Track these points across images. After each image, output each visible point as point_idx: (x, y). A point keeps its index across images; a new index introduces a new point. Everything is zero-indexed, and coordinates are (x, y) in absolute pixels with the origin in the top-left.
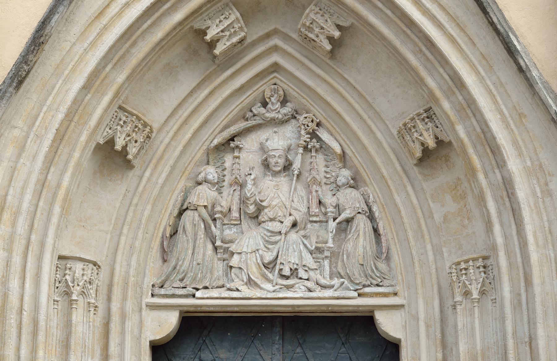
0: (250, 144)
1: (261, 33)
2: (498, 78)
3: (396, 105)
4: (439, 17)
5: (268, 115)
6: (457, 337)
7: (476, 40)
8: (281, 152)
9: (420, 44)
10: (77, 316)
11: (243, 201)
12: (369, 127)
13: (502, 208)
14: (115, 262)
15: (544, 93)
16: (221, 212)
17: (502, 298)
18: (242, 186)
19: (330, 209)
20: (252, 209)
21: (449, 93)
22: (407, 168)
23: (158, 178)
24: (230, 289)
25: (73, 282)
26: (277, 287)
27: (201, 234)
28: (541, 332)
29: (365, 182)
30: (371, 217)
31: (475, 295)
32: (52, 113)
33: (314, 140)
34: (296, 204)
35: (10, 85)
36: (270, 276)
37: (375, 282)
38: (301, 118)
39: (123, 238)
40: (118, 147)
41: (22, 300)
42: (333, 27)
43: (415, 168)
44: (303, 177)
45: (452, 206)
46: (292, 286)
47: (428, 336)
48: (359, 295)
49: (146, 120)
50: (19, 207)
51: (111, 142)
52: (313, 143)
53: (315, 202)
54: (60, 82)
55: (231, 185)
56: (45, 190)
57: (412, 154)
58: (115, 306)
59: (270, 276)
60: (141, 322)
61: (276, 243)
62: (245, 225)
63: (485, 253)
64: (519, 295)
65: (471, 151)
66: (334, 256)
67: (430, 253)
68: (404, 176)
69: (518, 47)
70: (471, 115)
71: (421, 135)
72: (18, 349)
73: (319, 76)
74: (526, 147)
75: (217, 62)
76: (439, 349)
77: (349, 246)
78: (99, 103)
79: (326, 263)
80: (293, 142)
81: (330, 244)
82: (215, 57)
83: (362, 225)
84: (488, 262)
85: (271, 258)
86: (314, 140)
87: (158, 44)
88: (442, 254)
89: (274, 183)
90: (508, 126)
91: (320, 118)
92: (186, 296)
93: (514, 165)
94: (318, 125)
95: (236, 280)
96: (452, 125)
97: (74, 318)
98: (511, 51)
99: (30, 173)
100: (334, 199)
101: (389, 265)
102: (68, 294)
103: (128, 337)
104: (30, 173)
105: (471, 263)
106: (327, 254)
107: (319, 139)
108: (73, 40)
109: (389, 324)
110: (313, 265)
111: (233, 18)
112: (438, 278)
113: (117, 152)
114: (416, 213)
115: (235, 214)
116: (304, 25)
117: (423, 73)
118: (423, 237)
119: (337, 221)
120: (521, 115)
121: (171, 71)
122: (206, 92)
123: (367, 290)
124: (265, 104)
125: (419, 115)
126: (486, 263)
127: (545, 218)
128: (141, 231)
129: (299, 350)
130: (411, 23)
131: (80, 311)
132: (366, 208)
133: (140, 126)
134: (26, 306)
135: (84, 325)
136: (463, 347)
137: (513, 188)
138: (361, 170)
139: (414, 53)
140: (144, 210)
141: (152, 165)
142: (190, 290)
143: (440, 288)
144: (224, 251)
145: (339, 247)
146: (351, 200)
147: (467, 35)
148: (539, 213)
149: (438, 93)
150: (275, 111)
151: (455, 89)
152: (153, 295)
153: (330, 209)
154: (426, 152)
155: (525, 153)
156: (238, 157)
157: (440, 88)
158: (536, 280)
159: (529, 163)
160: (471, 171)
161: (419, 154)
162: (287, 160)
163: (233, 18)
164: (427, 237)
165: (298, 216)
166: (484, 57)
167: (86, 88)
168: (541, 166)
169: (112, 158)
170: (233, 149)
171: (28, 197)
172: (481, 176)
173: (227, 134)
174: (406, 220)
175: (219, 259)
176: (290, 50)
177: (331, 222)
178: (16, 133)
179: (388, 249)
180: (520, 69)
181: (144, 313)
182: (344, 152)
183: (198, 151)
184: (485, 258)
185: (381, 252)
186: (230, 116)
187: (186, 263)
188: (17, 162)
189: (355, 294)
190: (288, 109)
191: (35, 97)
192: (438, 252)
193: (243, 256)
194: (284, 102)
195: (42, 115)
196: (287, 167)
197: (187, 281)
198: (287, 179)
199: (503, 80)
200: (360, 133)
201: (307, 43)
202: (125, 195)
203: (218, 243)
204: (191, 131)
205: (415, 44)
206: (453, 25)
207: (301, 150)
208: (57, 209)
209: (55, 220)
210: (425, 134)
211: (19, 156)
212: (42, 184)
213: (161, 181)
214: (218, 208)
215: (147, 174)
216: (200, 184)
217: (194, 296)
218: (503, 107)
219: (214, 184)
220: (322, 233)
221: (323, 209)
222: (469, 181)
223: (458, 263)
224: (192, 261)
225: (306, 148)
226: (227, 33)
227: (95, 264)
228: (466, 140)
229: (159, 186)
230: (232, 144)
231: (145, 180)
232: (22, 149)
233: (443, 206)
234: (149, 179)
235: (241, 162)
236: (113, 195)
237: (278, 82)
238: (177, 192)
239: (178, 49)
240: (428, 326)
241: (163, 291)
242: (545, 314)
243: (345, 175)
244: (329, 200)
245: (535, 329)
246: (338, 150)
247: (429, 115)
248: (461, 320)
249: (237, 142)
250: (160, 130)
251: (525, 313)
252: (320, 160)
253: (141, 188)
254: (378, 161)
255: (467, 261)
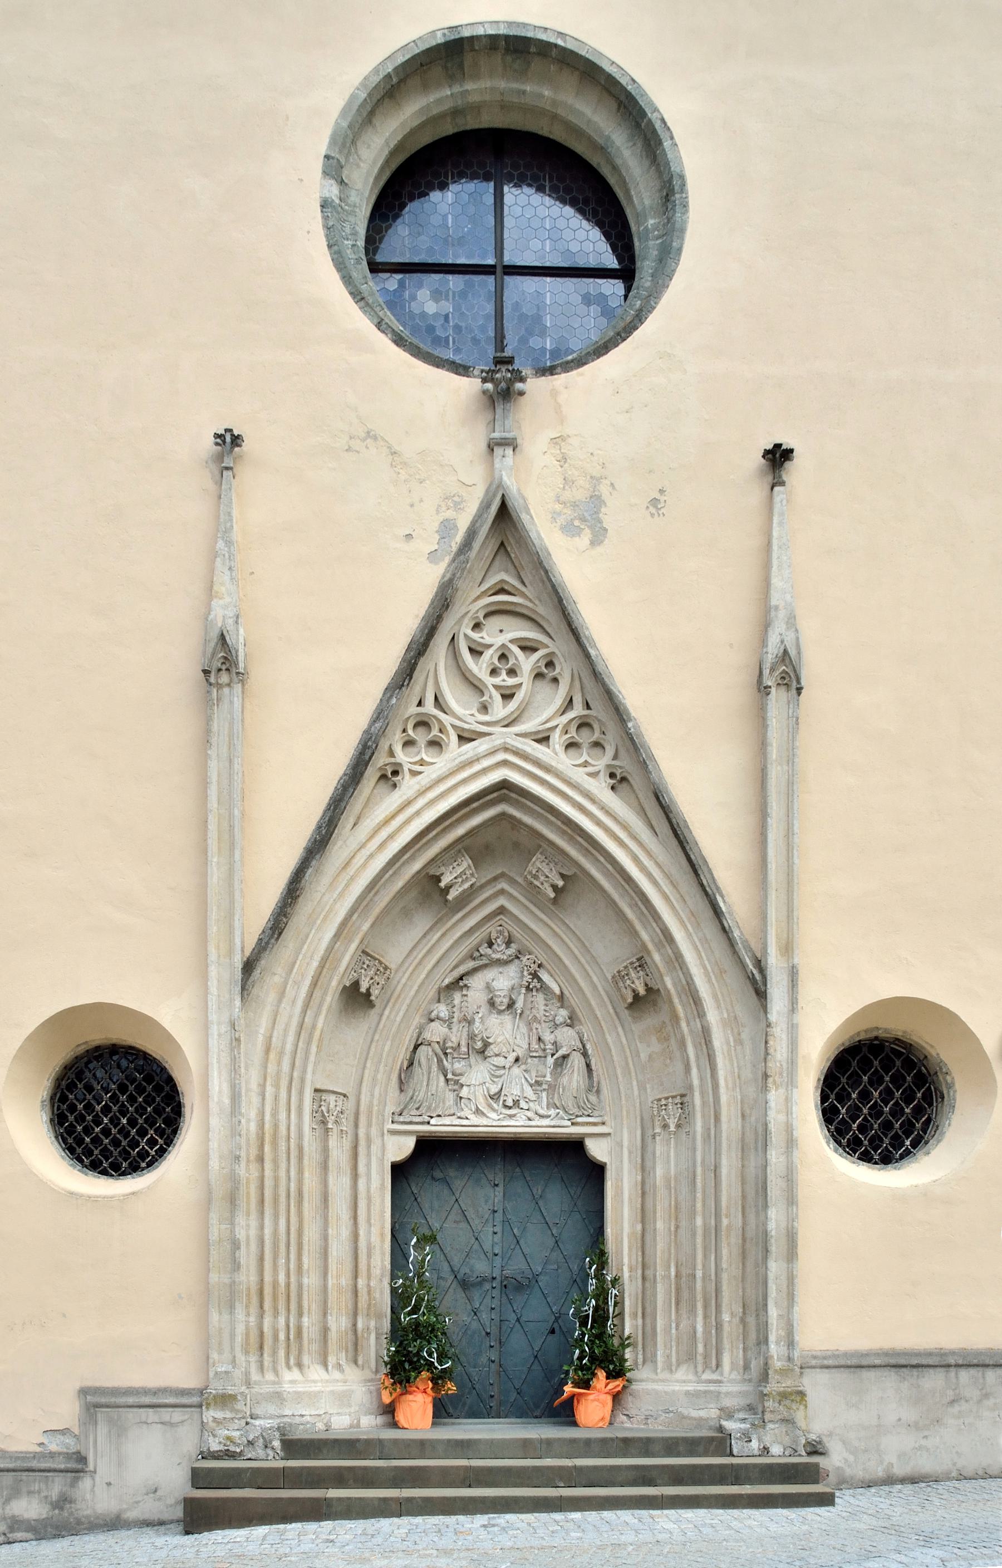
0: (477, 983)
1: (489, 877)
2: (704, 935)
3: (610, 952)
4: (655, 874)
5: (494, 956)
6: (654, 1163)
7: (687, 898)
8: (505, 993)
9: (637, 899)
10: (333, 1142)
11: (472, 1037)
12: (585, 970)
13: (699, 1053)
14: (360, 1093)
15: (743, 953)
16: (452, 1048)
17: (695, 1132)
18: (470, 1022)
19: (549, 1046)
20: (479, 1045)
21: (659, 946)
22: (618, 1010)
23: (396, 1016)
24: (459, 1118)
25: (328, 1112)
26: (502, 1116)
27: (435, 1068)
28: (724, 1162)
29: (580, 1021)
30: (585, 1054)
31: (672, 1128)
32: (307, 961)
33: (535, 980)
34: (518, 1041)
35: (272, 936)
36: (495, 1106)
37: (586, 1113)
38: (524, 959)
39: (367, 1072)
40: (363, 990)
41: (289, 1129)
42: (558, 876)
43: (626, 1011)
44: (524, 1015)
45: (656, 1047)
46: (514, 1115)
47: (630, 1161)
48: (573, 1124)
49: (387, 964)
50: (283, 1047)
51: (356, 984)
52: (534, 984)
53: (535, 1038)
54: (313, 931)
55: (460, 1022)
56: (303, 1032)
57: (624, 999)
58: (362, 1132)
59: (495, 1106)
60: (383, 1145)
61: (501, 1076)
62: (472, 1060)
63: (682, 1091)
64: (709, 1129)
65: (676, 1001)
66: (552, 1088)
67: (636, 1088)
68: (615, 1017)
69: (724, 909)
70: (678, 968)
71: (633, 983)
72: (288, 1171)
73: (541, 920)
74: (724, 1000)
75: (449, 905)
76: (639, 1173)
77: (565, 1080)
78: (346, 950)
79: (544, 1094)
80: (516, 981)
81: (548, 1078)
82: (446, 901)
83: (576, 1062)
84: (685, 1099)
85: (497, 1090)
86: (535, 980)
87: (399, 892)
88: (645, 1090)
89: (498, 1021)
90: (709, 981)
91: (542, 959)
92: (422, 1123)
93: (713, 1016)
94: (540, 966)
95: (466, 1109)
96: (661, 976)
97: (330, 1143)
98: (717, 912)
99: (291, 1017)
100: (552, 1036)
101: (598, 1097)
102: (324, 1122)
103: (374, 1159)
104: (291, 1017)
105: (670, 1100)
106: (545, 1086)
107: (540, 980)
108: (323, 891)
109: (597, 1150)
110: (533, 1097)
111: (465, 865)
112: (641, 1111)
113: (362, 993)
114: (624, 1052)
115: (464, 1049)
116: (530, 873)
117: (638, 927)
118: (630, 1073)
119: (555, 1057)
120: (722, 972)
121: (406, 913)
122: (439, 934)
123: (579, 1120)
124: (490, 944)
125: (632, 963)
126: (683, 1101)
127: (735, 1065)
128: (382, 1065)
129: (518, 1170)
130: (628, 879)
131: (335, 1137)
132: (581, 1046)
133: (382, 969)
134: (292, 1135)
135: (339, 1150)
136: (659, 1172)
137: (710, 1036)
138: (577, 1010)
139: (631, 906)
140: (384, 1045)
141: (390, 1004)
142: (427, 1119)
143: (642, 1119)
144: (454, 1083)
145: (556, 1080)
146: (567, 1038)
147: (679, 893)
148: (731, 1060)
149: (650, 946)
150: (500, 952)
151: (666, 944)
152: (393, 1122)
153: (549, 1046)
154: (636, 997)
155: (722, 1005)
156: (466, 995)
157: (652, 941)
158: (724, 1118)
159: (726, 1015)
160: (675, 1018)
161: (630, 1000)
162: (511, 999)
163: (465, 865)
164: (633, 1074)
165: (520, 1052)
166: (693, 914)
167: (337, 936)
168: (736, 1018)
169: (356, 998)
170: (462, 988)
171: (291, 1039)
172: (683, 1024)
173: (456, 974)
174: (615, 1058)
175: (450, 1090)
176: (515, 893)
177: (549, 1057)
178: (277, 979)
179: (599, 1083)
180: (724, 929)
181: (386, 1137)
182: (562, 993)
183: (432, 993)
184: (682, 1096)
185: (593, 1087)
186: (460, 956)
187: (422, 1094)
188: (278, 1006)
189: (569, 1123)
190: (512, 951)
191: (291, 945)
192: (642, 1087)
193: (472, 1088)
194: (508, 943)
195: (298, 962)
196: (511, 1005)
197: (423, 1110)
198: (510, 1017)
199: (709, 937)
200: (578, 976)
201: (532, 891)
202: (367, 1032)
203: (450, 1076)
204: (425, 972)
205: (632, 898)
206: (667, 882)
207: (523, 991)
208: (314, 1049)
209: (312, 1058)
210: (637, 982)
211: (280, 1001)
212: (301, 1025)
213: (398, 1019)
214: (449, 1044)
215: (387, 1012)
216: (432, 1021)
217: (429, 1123)
218: (706, 962)
219: (445, 1021)
220: (541, 1068)
221: (542, 1046)
222: (673, 1026)
223: (660, 1100)
224: (427, 1092)
225: (528, 988)
226: (460, 880)
227: (345, 1096)
228: (673, 991)
229: (397, 1023)
230: (461, 984)
231: (384, 1017)
232: (282, 994)
233: (649, 1046)
234: (388, 1017)
235: (469, 999)
236: (356, 1033)
237: (504, 924)
238: (412, 1028)
239: (414, 893)
240: (630, 1153)
241: (401, 1119)
242: (729, 1147)
243: (563, 1014)
244: (548, 1037)
245: (720, 1158)
246: (557, 991)
247: (641, 964)
248: (659, 1149)
249: (465, 982)
250: (397, 971)
251: (713, 1145)
252: (540, 998)
253: (381, 1026)
254: (593, 1003)
255: (667, 1098)
